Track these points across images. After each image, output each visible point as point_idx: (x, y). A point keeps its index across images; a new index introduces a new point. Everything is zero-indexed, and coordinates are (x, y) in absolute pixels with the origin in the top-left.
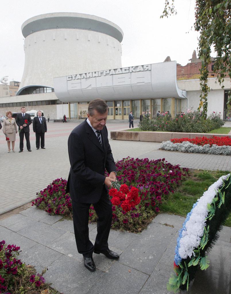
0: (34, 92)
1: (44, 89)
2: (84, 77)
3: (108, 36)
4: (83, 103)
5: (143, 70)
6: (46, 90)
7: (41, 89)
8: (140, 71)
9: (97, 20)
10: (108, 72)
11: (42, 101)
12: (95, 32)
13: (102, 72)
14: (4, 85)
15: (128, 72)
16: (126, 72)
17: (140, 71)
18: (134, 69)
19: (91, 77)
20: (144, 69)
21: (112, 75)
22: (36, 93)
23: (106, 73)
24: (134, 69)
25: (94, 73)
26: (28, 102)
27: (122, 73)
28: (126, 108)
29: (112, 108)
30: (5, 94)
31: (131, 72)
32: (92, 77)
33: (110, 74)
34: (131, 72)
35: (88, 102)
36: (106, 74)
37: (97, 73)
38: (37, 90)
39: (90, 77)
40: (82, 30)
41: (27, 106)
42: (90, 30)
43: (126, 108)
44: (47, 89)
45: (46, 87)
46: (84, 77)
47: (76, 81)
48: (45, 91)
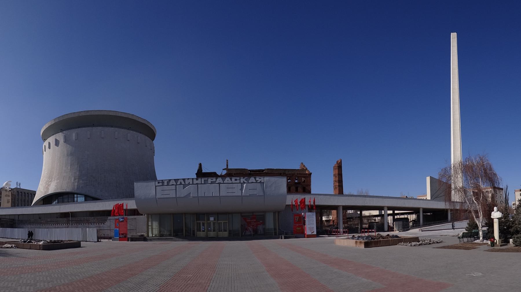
1: (74, 196)
3: (147, 137)
6: (77, 197)
7: (64, 196)
16: (159, 185)
17: (252, 183)
21: (219, 183)
27: (232, 183)
39: (189, 184)
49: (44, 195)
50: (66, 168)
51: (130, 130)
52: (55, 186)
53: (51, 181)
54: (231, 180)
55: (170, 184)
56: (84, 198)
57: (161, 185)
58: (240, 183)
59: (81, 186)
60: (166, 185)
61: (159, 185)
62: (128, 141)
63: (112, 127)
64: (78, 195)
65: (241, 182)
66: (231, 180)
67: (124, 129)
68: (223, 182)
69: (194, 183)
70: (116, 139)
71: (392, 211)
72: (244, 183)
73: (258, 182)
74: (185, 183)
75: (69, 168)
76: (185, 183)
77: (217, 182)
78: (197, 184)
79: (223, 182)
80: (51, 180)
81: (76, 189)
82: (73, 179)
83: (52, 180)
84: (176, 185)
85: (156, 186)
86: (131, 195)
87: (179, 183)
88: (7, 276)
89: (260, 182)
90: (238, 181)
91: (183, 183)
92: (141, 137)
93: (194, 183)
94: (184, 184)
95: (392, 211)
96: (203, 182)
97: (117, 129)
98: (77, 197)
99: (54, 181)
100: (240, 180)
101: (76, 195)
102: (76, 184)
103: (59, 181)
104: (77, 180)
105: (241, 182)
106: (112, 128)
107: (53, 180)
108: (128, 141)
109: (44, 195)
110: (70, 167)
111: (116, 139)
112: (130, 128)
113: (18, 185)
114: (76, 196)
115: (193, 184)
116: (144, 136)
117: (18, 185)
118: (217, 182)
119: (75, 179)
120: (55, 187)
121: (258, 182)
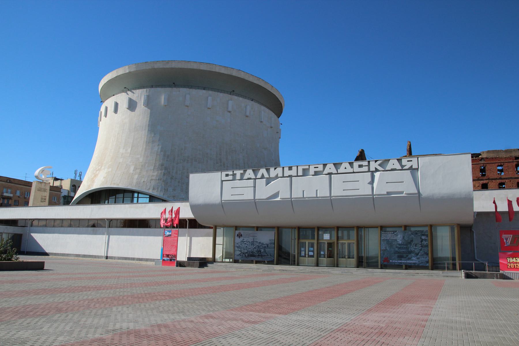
0: (112, 199)
1: (133, 195)
2: (263, 175)
3: (263, 108)
4: (263, 229)
5: (401, 168)
6: (138, 197)
7: (126, 195)
8: (392, 170)
9: (246, 79)
10: (321, 168)
11: (111, 220)
12: (241, 99)
13: (307, 167)
14: (41, 182)
15: (367, 170)
16: (227, 178)
17: (392, 170)
18: (380, 165)
19: (279, 176)
20: (402, 166)
21: (330, 174)
22: (115, 203)
23: (316, 170)
24: (380, 165)
25: (286, 169)
26: (107, 219)
27: (354, 172)
28: (345, 243)
29: (312, 241)
30: (40, 200)
31: (374, 170)
32: (281, 176)
33: (326, 172)
34: (374, 170)
35: (449, 226)
36: (315, 172)
37: (294, 168)
38: (118, 196)
39: (277, 177)
40: (219, 93)
41: (186, 228)
42: (233, 95)
43: (305, 243)
44: (140, 195)
45: (138, 193)
46: (263, 175)
47: (244, 183)
48: (135, 200)
49: (86, 190)
50: (124, 150)
51: (233, 95)
52: (104, 178)
53: (99, 170)
54: (352, 167)
55: (244, 178)
56: (148, 199)
57: (231, 179)
58: (369, 171)
59: (142, 181)
60: (239, 179)
61: (227, 178)
62: (230, 112)
63: (204, 90)
64: (140, 195)
65: (371, 170)
66: (352, 167)
67: (242, 98)
68: (336, 172)
69: (285, 176)
70: (209, 108)
71: (192, 176)
72: (377, 170)
73: (404, 168)
74: (269, 175)
75: (129, 150)
76: (269, 175)
77: (324, 173)
78: (290, 176)
79: (337, 171)
80: (100, 167)
81: (134, 185)
82: (132, 168)
83: (101, 168)
84: (255, 179)
85: (222, 181)
86: (185, 198)
87: (259, 176)
88: (104, 304)
89: (411, 168)
90: (365, 169)
91: (266, 175)
92: (266, 113)
93: (285, 176)
94: (268, 177)
95: (192, 176)
96: (300, 173)
97: (210, 92)
98: (138, 197)
99: (104, 169)
100: (369, 165)
101: (137, 194)
102: (136, 176)
103: (110, 169)
104: (138, 171)
105: (371, 170)
106: (203, 91)
107: (103, 168)
108: (230, 112)
109: (86, 190)
110: (130, 149)
111: (209, 108)
112: (234, 91)
113: (78, 175)
114: (136, 195)
115: (283, 177)
116: (259, 105)
117: (78, 175)
118: (324, 173)
119: (135, 169)
120: (104, 179)
121: (404, 168)
